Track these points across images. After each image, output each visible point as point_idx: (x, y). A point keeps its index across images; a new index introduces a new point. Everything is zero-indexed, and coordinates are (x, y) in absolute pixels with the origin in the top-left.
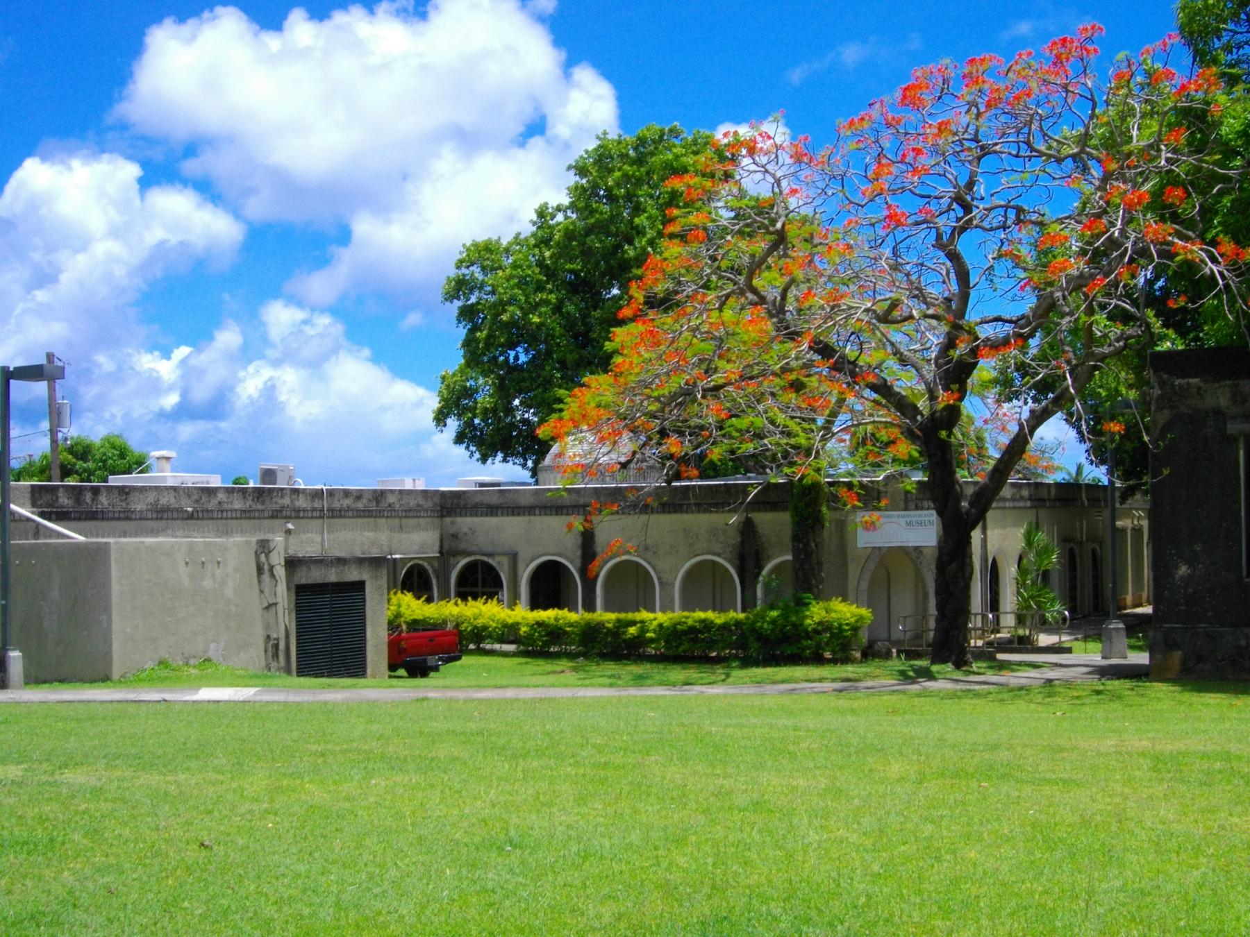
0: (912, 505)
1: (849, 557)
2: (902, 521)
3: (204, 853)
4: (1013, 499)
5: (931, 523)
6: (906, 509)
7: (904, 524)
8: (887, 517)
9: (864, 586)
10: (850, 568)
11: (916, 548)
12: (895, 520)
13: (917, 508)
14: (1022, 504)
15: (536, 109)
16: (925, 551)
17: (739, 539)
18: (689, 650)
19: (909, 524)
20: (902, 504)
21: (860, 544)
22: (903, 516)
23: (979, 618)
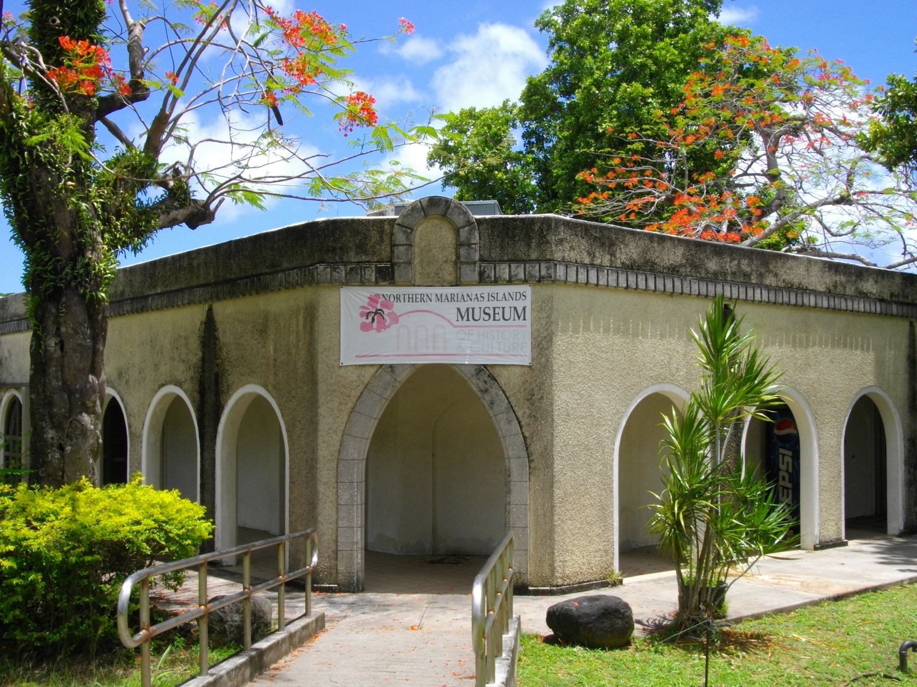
0: (471, 273)
1: (322, 388)
2: (450, 310)
3: (418, 633)
4: (829, 293)
5: (519, 314)
6: (457, 283)
7: (453, 315)
8: (412, 299)
9: (358, 450)
10: (322, 410)
11: (481, 369)
12: (433, 305)
13: (483, 280)
14: (861, 306)
15: (465, 51)
16: (503, 377)
17: (200, 354)
18: (795, 513)
19: (466, 315)
20: (448, 272)
21: (347, 358)
22: (452, 298)
23: (209, 606)
